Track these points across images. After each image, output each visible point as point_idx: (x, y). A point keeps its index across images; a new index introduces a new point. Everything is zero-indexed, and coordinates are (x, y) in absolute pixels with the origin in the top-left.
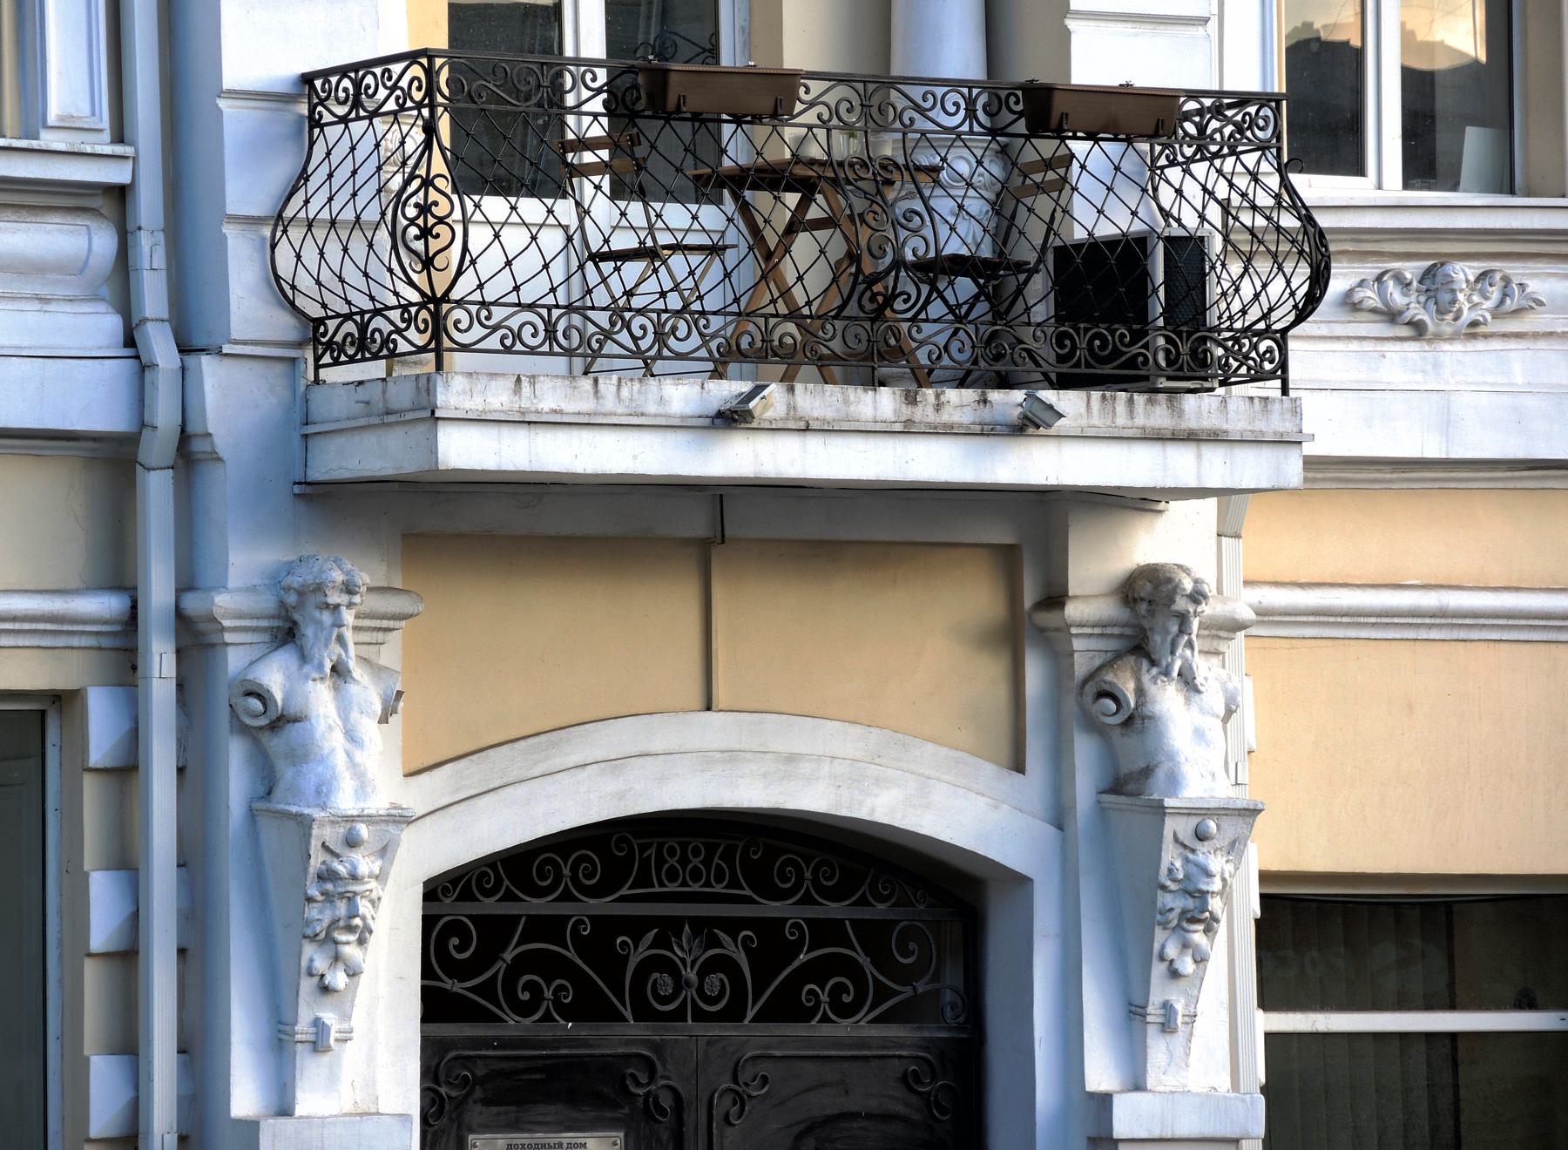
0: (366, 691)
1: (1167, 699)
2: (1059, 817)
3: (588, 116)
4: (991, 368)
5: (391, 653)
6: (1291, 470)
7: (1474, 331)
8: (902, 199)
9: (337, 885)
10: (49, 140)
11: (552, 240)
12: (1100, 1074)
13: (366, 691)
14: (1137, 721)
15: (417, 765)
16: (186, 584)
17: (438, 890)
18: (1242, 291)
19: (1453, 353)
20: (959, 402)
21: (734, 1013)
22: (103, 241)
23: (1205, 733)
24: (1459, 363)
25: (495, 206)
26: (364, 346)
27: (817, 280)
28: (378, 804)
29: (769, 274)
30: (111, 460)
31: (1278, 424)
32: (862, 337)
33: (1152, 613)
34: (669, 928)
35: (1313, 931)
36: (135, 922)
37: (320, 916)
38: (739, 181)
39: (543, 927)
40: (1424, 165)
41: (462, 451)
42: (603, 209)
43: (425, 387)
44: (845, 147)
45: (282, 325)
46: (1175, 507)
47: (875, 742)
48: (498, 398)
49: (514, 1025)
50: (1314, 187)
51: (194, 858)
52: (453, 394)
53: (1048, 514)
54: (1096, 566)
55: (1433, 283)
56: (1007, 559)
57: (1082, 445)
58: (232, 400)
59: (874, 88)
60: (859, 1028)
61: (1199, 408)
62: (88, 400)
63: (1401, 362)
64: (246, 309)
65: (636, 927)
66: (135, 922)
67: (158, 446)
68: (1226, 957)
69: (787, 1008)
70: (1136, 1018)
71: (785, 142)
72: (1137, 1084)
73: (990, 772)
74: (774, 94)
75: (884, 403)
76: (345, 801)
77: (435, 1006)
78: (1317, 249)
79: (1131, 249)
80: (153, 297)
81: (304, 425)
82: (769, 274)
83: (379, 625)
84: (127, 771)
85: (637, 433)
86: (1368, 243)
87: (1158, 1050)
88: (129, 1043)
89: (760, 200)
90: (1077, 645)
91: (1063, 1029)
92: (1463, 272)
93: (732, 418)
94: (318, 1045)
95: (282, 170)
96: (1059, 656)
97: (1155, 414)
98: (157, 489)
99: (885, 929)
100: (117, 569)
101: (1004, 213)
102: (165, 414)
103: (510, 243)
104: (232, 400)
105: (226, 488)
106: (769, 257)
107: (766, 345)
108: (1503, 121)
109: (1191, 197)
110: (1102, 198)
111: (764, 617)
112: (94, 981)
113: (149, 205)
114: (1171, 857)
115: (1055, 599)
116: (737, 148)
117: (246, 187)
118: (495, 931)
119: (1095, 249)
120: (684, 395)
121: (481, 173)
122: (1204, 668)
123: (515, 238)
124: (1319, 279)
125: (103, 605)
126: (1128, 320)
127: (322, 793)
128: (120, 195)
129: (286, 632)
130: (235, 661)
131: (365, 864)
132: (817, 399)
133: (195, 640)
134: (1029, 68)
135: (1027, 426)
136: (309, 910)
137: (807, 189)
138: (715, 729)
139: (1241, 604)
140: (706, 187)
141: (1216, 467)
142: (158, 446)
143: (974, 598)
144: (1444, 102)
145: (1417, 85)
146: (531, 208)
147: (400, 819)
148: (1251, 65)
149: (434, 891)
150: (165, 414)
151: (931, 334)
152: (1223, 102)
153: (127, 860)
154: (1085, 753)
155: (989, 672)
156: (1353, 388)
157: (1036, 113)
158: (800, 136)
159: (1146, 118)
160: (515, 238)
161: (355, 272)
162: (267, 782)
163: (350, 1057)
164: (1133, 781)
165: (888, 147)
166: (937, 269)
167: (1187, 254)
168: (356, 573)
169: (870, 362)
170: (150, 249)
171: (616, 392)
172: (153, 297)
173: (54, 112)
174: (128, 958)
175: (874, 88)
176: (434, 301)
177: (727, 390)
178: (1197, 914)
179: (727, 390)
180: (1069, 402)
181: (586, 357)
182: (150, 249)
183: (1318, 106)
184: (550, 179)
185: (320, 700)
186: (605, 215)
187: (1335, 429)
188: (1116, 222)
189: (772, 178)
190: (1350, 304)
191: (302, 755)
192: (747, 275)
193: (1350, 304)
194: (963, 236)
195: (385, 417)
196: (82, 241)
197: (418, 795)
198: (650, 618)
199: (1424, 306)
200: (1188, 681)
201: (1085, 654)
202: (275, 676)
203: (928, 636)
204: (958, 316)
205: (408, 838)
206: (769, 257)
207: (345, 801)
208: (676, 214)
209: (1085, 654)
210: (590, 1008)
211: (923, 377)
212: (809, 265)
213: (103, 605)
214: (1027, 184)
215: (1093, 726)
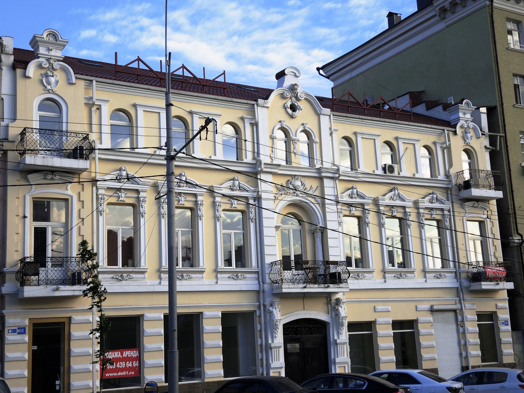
0: (278, 310)
1: (340, 308)
2: (332, 318)
3: (293, 264)
4: (325, 283)
5: (279, 307)
6: (348, 290)
7: (361, 279)
8: (317, 270)
9: (276, 325)
10: (141, 267)
11: (291, 274)
12: (336, 338)
13: (278, 310)
14: (338, 310)
15: (282, 316)
16: (264, 302)
17: (284, 325)
18: (344, 276)
19: (124, 282)
20: (322, 285)
21: (307, 334)
22: (257, 275)
23: (343, 311)
24: (238, 282)
25: (286, 271)
26: (276, 283)
27: (311, 276)
28: (279, 318)
29: (307, 276)
30: (258, 292)
31: (347, 286)
32: (315, 281)
33: (338, 301)
34: (302, 328)
35: (352, 326)
36: (261, 328)
37: (275, 327)
38: (305, 269)
39: (292, 328)
40: (357, 266)
41: (284, 291)
42: (294, 271)
43: (281, 286)
44: (313, 266)
45: (270, 281)
46: (501, 292)
47: (317, 313)
48: (287, 286)
49: (290, 335)
50: (348, 268)
51: (265, 323)
52: (283, 286)
53: (330, 294)
54: (334, 298)
55: (358, 275)
56: (327, 298)
57: (332, 288)
58: (266, 287)
59: (315, 262)
60: (317, 335)
61: (341, 285)
62: (255, 288)
63: (356, 281)
64: (268, 280)
65: (299, 327)
66: (261, 328)
67: (261, 291)
68: (345, 328)
69: (311, 333)
70: (338, 334)
71: (308, 266)
72: (339, 338)
73: (326, 314)
74: (307, 262)
75: (317, 286)
76: (276, 318)
77: (284, 334)
78: (349, 273)
79: (335, 273)
80: (261, 280)
81: (272, 289)
82: (307, 276)
83: (278, 304)
84: (260, 316)
85: (298, 289)
86: (353, 272)
87: (340, 336)
88: (261, 338)
89: (306, 270)
90: (332, 303)
91: (333, 335)
92: (360, 274)
93: (305, 287)
94: (275, 337)
95: (270, 269)
96: (331, 305)
97: (338, 286)
98: (261, 294)
99: (320, 327)
100: (259, 301)
101: (325, 270)
102: (262, 288)
103: (287, 274)
104: (266, 287)
105: (266, 294)
106: (307, 275)
107: (307, 282)
108: (362, 263)
109: (339, 269)
110: (333, 269)
111: (308, 303)
112: (258, 333)
113: (260, 273)
114: (340, 321)
115: (331, 301)
116: (304, 266)
117: (267, 271)
118: (289, 328)
119: (332, 273)
120: (301, 286)
121: (284, 269)
122: (342, 306)
123: (288, 274)
124: (349, 275)
125: (258, 304)
126: (335, 279)
127: (275, 318)
128: (258, 272)
129: (271, 305)
130: (268, 307)
131: (278, 323)
132: (312, 286)
133: (265, 306)
134: (326, 260)
135: (328, 287)
136: (274, 327)
137: (310, 269)
138: (305, 312)
139: (345, 301)
140: (302, 269)
141: (342, 290)
142: (261, 291)
143: (324, 301)
144: (358, 261)
145: (356, 260)
146: (289, 271)
147: (281, 320)
148: (343, 259)
149: (284, 325)
150: (262, 288)
151: (320, 280)
152: (341, 262)
153: (260, 324)
154: (333, 313)
155: (326, 307)
156: (352, 283)
157: (327, 263)
158: (309, 265)
159: (335, 263)
160: (288, 274)
161: (277, 277)
162: (270, 317)
163: (278, 338)
164: (337, 314)
165: (316, 266)
166: (320, 275)
167: (339, 273)
168: (276, 300)
169: (315, 283)
170: (260, 276)
171: (296, 286)
172: (261, 280)
173: (253, 266)
174: (261, 331)
175: (315, 262)
176: (282, 279)
177: (304, 285)
178: (343, 325)
179: (304, 285)
180: (331, 285)
181: (293, 283)
182: (260, 276)
183: (348, 261)
184: (290, 269)
185: (274, 310)
186: (294, 272)
187: (351, 287)
188: (334, 271)
189: (307, 268)
190: (352, 277)
191: (273, 315)
192: (306, 276)
193: (352, 277)
194: (322, 272)
195: (278, 288)
196: (255, 276)
197: (282, 318)
198: (299, 303)
199: (358, 277)
200: (341, 307)
201: (333, 305)
202: (271, 309)
203: (321, 304)
204: (322, 279)
205: (281, 321)
206: (307, 275)
207: (276, 318)
208: (300, 272)
209: (333, 305)
210: (296, 334)
211: (320, 284)
212: (310, 275)
213: (258, 304)
214: (327, 268)
215: (334, 310)
